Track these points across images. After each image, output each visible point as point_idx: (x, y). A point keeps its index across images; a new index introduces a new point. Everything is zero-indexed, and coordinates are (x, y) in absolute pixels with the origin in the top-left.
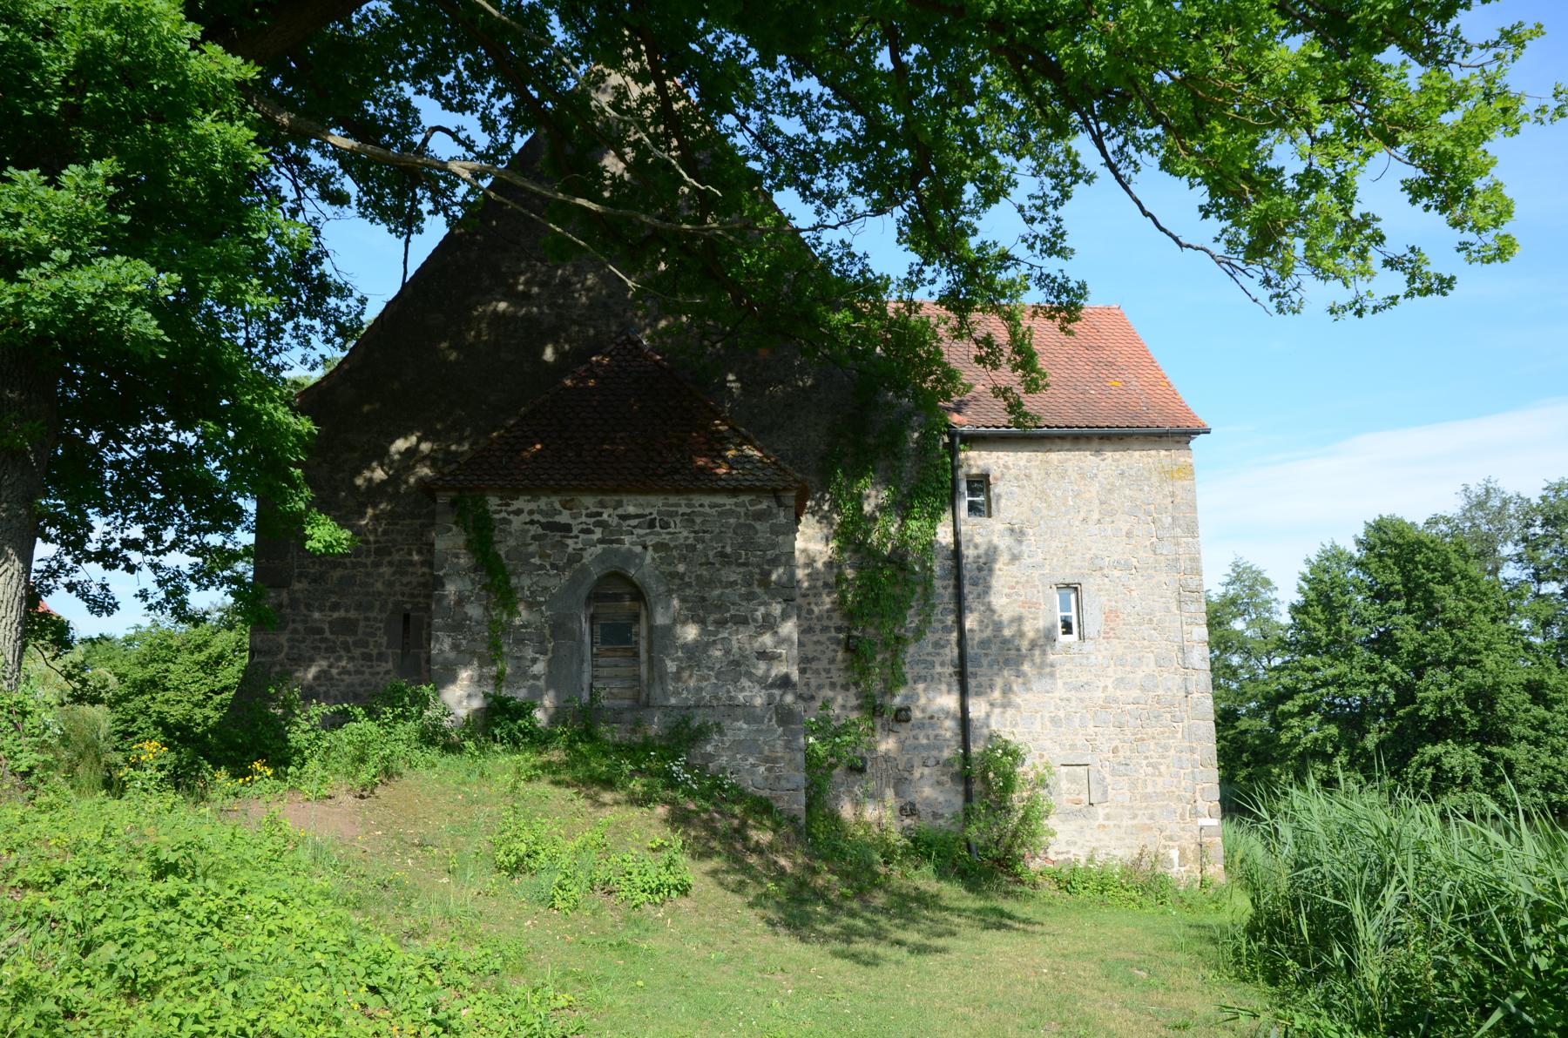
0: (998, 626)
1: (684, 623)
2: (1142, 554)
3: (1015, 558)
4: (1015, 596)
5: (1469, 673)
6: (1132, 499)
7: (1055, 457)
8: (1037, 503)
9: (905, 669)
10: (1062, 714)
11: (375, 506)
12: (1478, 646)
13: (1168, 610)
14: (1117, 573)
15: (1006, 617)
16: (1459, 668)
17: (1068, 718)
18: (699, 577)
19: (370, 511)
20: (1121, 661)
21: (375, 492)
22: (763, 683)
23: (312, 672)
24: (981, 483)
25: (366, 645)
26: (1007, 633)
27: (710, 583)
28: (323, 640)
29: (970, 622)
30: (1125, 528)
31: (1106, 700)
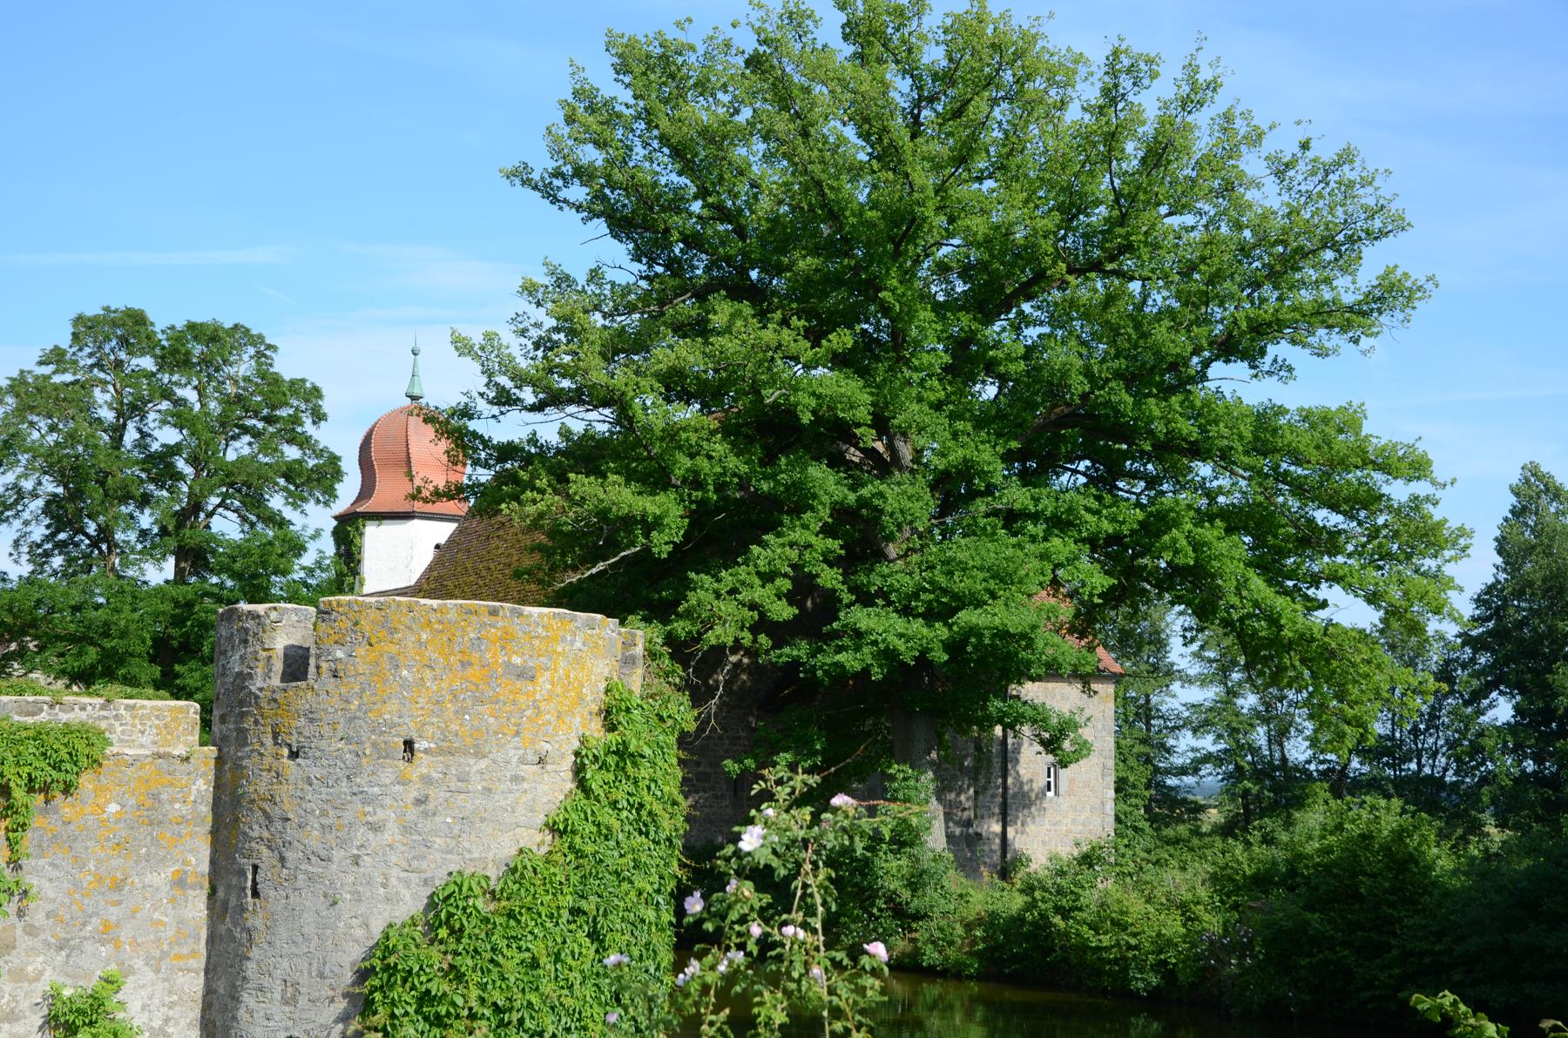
0: (1022, 783)
20: (1074, 809)
26: (1026, 788)
29: (1010, 781)
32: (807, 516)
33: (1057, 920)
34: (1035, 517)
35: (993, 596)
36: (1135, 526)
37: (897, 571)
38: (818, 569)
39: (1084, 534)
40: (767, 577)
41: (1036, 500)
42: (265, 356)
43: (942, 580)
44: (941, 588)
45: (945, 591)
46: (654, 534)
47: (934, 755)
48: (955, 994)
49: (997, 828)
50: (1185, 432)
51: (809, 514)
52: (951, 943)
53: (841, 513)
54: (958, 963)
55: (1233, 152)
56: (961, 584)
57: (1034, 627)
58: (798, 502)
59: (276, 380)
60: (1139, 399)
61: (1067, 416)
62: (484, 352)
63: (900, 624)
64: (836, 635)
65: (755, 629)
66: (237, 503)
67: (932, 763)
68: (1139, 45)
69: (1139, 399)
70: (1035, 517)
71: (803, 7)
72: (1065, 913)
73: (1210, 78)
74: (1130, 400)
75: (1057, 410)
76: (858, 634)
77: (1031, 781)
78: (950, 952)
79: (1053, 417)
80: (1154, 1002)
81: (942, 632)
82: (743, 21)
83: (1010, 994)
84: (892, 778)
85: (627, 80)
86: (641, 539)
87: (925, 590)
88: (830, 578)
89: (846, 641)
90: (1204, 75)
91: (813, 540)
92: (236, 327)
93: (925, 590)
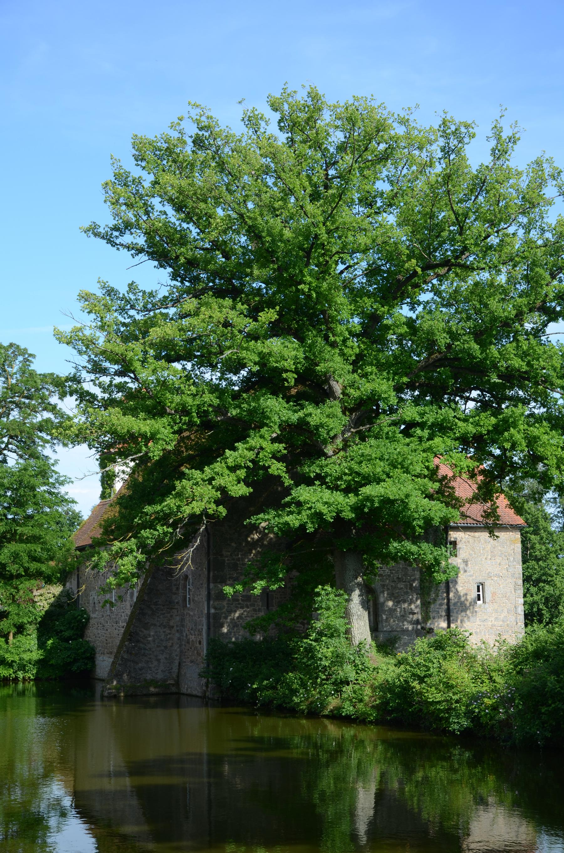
0: (459, 597)
1: (388, 600)
2: (504, 572)
3: (465, 571)
4: (465, 586)
5: (547, 587)
6: (501, 551)
7: (477, 534)
8: (471, 552)
9: (431, 614)
10: (478, 630)
11: (255, 549)
12: (552, 572)
13: (511, 592)
14: (496, 579)
15: (462, 594)
16: (541, 584)
17: (480, 632)
18: (392, 586)
19: (254, 552)
20: (496, 611)
21: (255, 544)
22: (411, 622)
23: (237, 615)
24: (454, 543)
25: (254, 605)
26: (463, 599)
27: (396, 588)
28: (239, 604)
29: (451, 595)
30: (499, 561)
31: (492, 625)
32: (264, 430)
33: (415, 684)
34: (422, 425)
35: (389, 476)
36: (490, 428)
37: (334, 464)
38: (270, 463)
39: (458, 435)
40: (233, 469)
41: (422, 415)
42: (28, 360)
43: (356, 467)
44: (356, 473)
45: (358, 474)
46: (151, 444)
47: (360, 579)
48: (369, 734)
49: (444, 625)
50: (517, 366)
51: (266, 428)
52: (361, 701)
53: (286, 426)
54: (364, 713)
55: (542, 184)
56: (365, 469)
57: (407, 496)
58: (254, 422)
59: (32, 374)
60: (484, 345)
61: (440, 360)
62: (73, 340)
63: (327, 495)
64: (288, 505)
65: (218, 503)
66: (14, 448)
67: (359, 585)
68: (459, 116)
69: (484, 345)
70: (422, 425)
71: (256, 113)
72: (421, 680)
73: (510, 135)
74: (477, 347)
75: (434, 356)
76: (299, 504)
77: (466, 594)
78: (360, 706)
79: (431, 361)
80: (467, 738)
81: (352, 499)
82: (186, 116)
83: (393, 735)
84: (318, 594)
85: (144, 164)
86: (144, 448)
87: (345, 474)
88: (277, 468)
89: (293, 508)
90: (313, 86)
91: (265, 444)
92: (11, 345)
93: (345, 474)
